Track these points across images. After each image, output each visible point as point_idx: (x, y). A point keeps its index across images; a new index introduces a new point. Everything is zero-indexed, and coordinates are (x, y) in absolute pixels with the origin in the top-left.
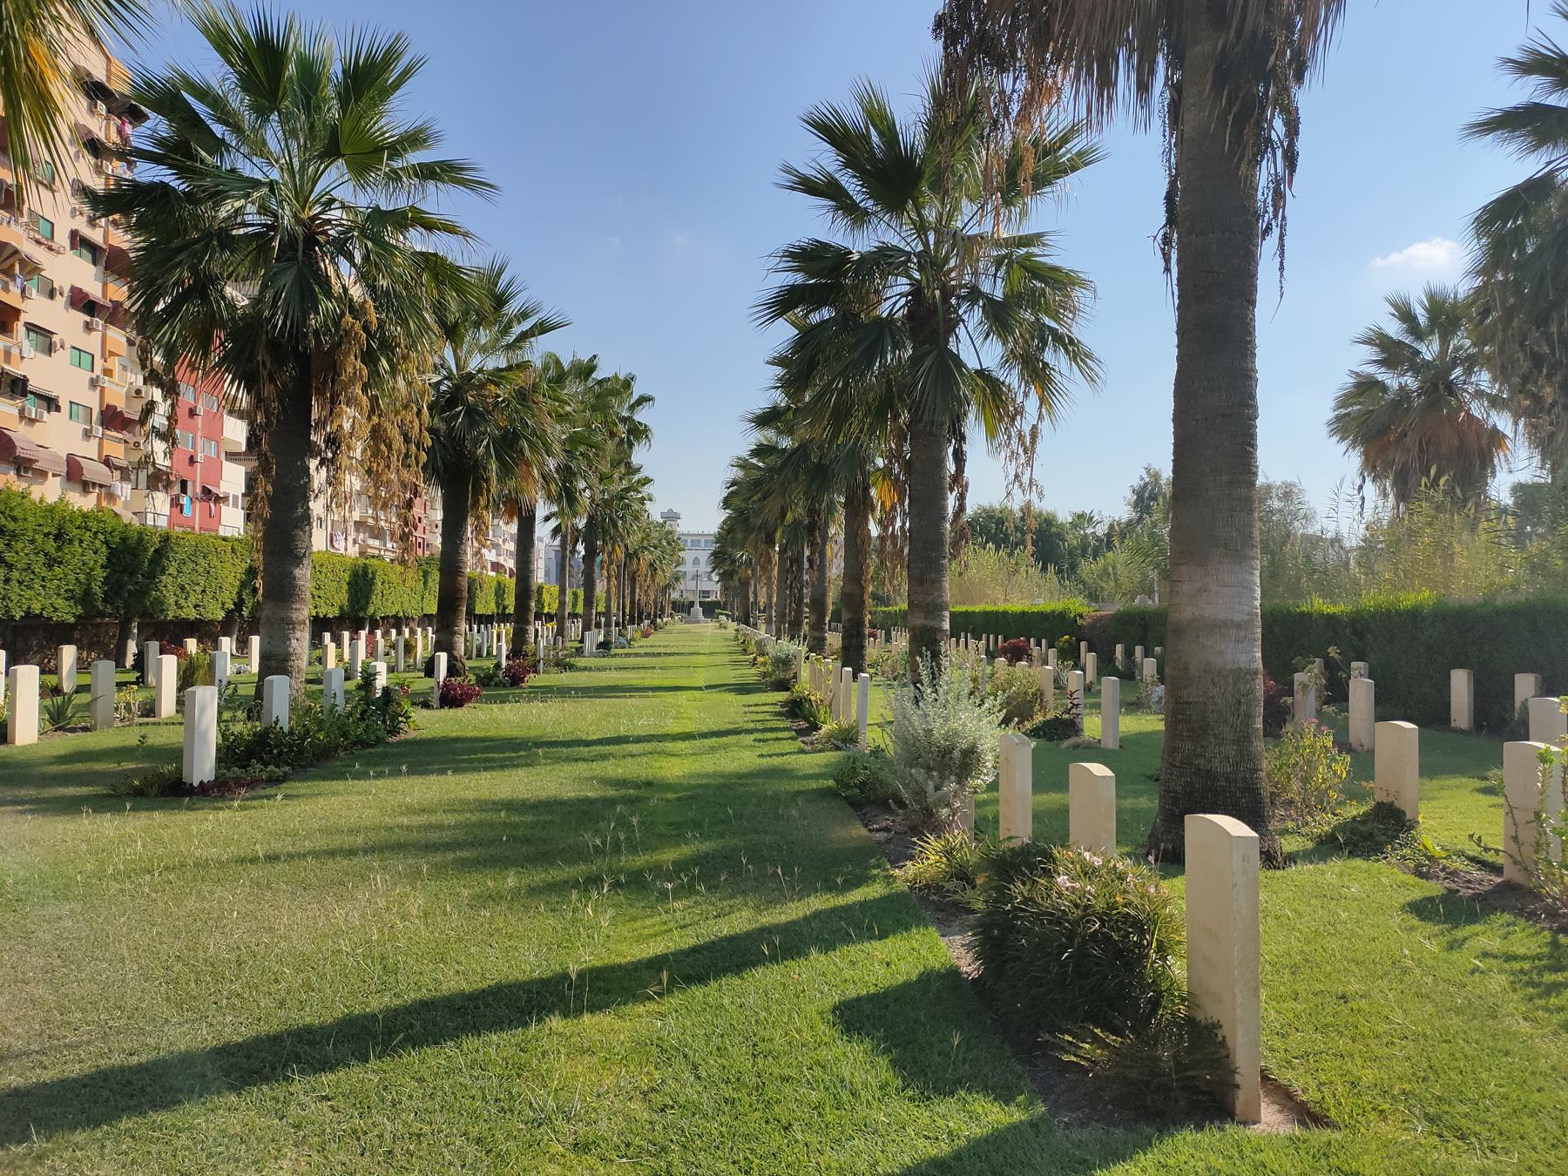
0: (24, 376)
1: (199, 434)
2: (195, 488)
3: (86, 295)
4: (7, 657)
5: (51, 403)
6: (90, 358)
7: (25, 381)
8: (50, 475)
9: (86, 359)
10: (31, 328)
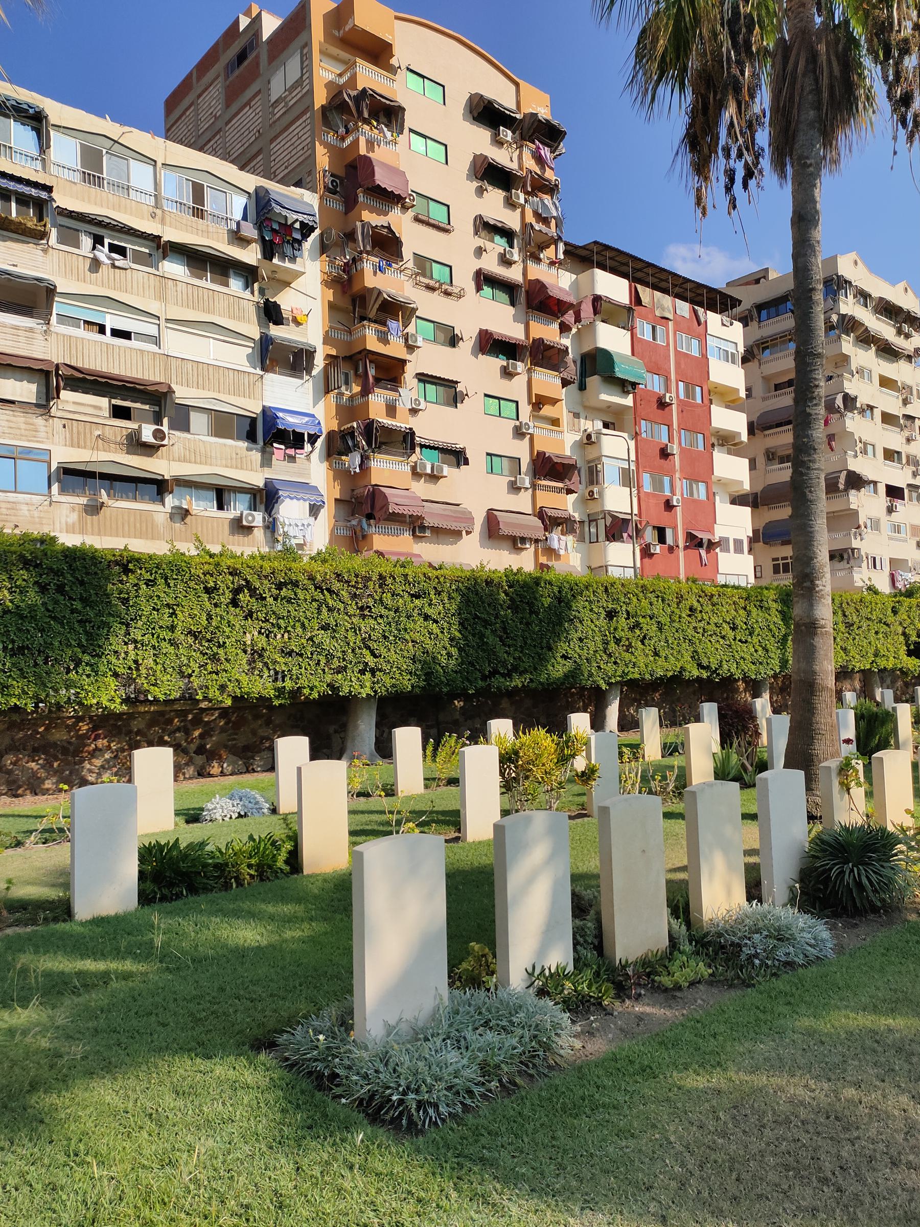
0: (411, 429)
1: (678, 475)
2: (677, 536)
3: (491, 334)
4: (423, 733)
5: (458, 457)
6: (514, 405)
7: (411, 433)
8: (464, 533)
9: (508, 409)
10: (424, 378)
